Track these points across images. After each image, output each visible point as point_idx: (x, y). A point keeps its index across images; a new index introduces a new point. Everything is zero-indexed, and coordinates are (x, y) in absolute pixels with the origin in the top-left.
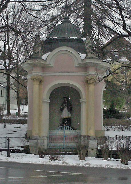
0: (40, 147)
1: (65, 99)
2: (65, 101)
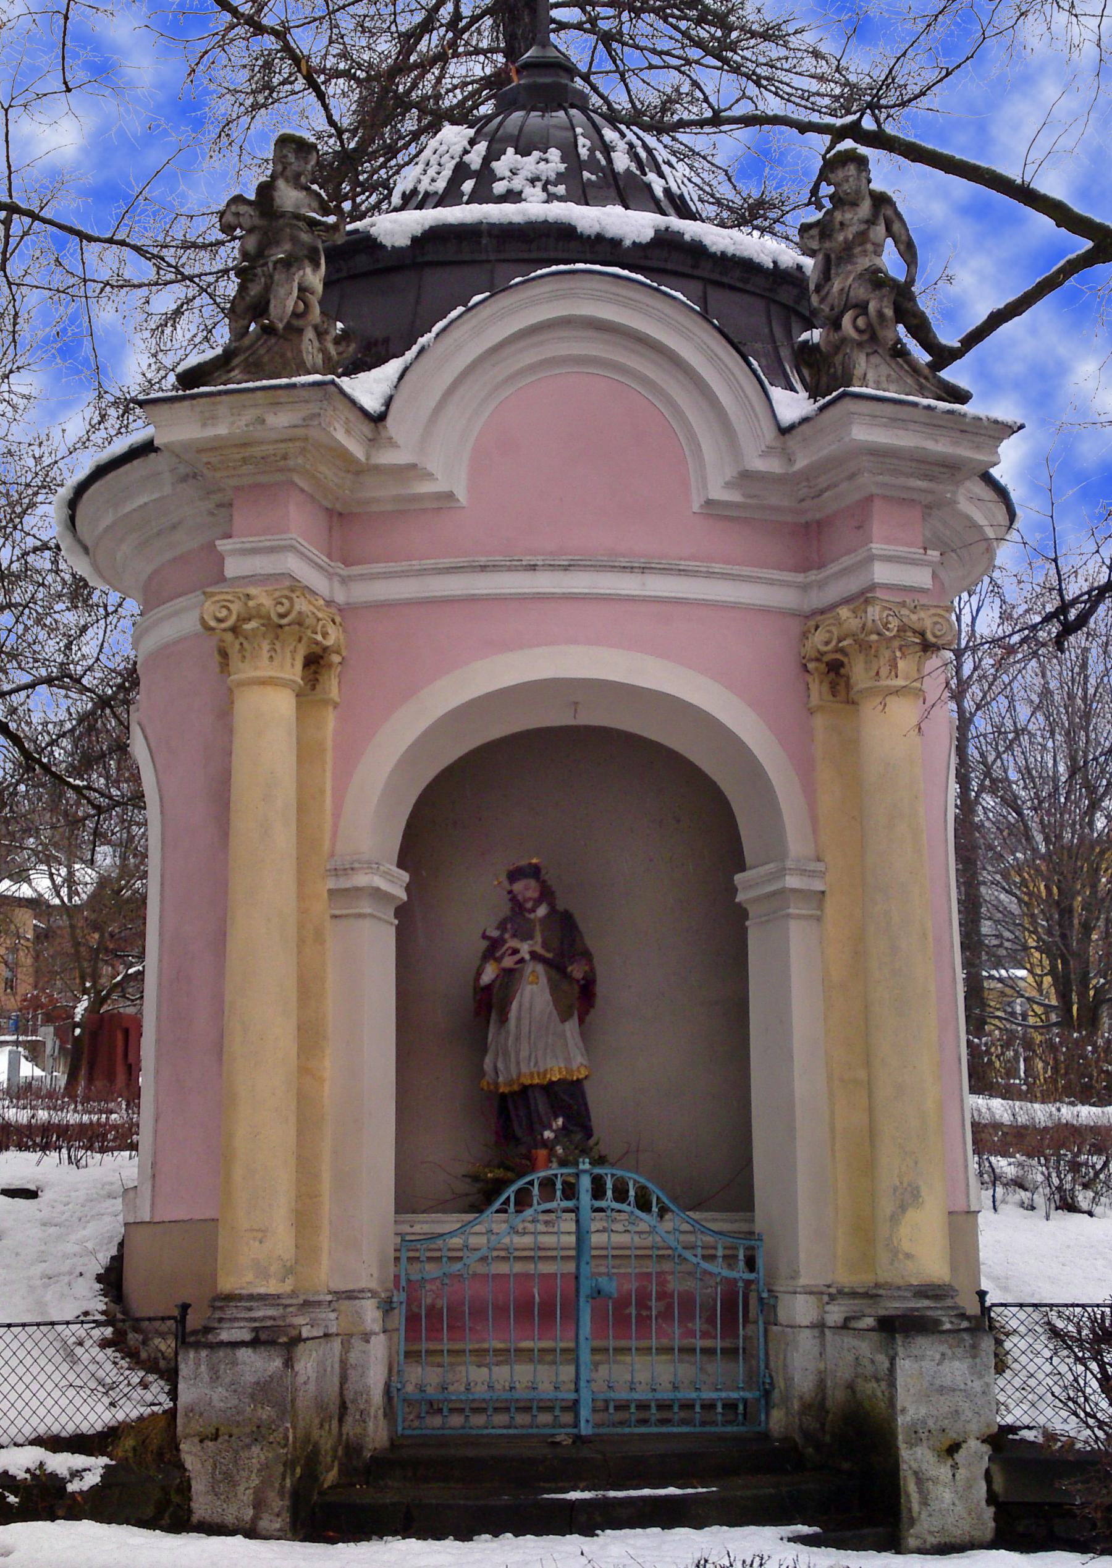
0: (307, 1439)
1: (527, 889)
2: (518, 906)
